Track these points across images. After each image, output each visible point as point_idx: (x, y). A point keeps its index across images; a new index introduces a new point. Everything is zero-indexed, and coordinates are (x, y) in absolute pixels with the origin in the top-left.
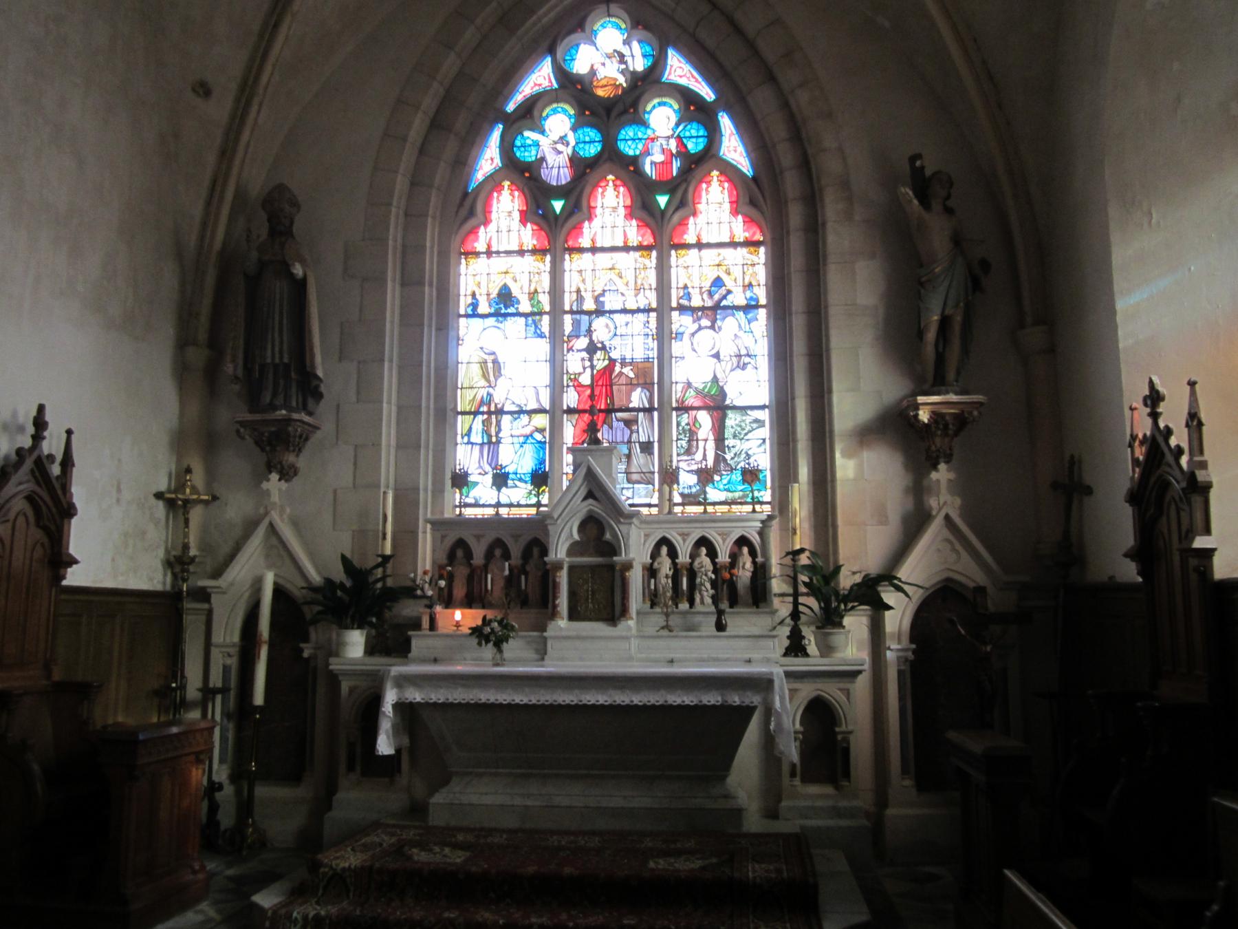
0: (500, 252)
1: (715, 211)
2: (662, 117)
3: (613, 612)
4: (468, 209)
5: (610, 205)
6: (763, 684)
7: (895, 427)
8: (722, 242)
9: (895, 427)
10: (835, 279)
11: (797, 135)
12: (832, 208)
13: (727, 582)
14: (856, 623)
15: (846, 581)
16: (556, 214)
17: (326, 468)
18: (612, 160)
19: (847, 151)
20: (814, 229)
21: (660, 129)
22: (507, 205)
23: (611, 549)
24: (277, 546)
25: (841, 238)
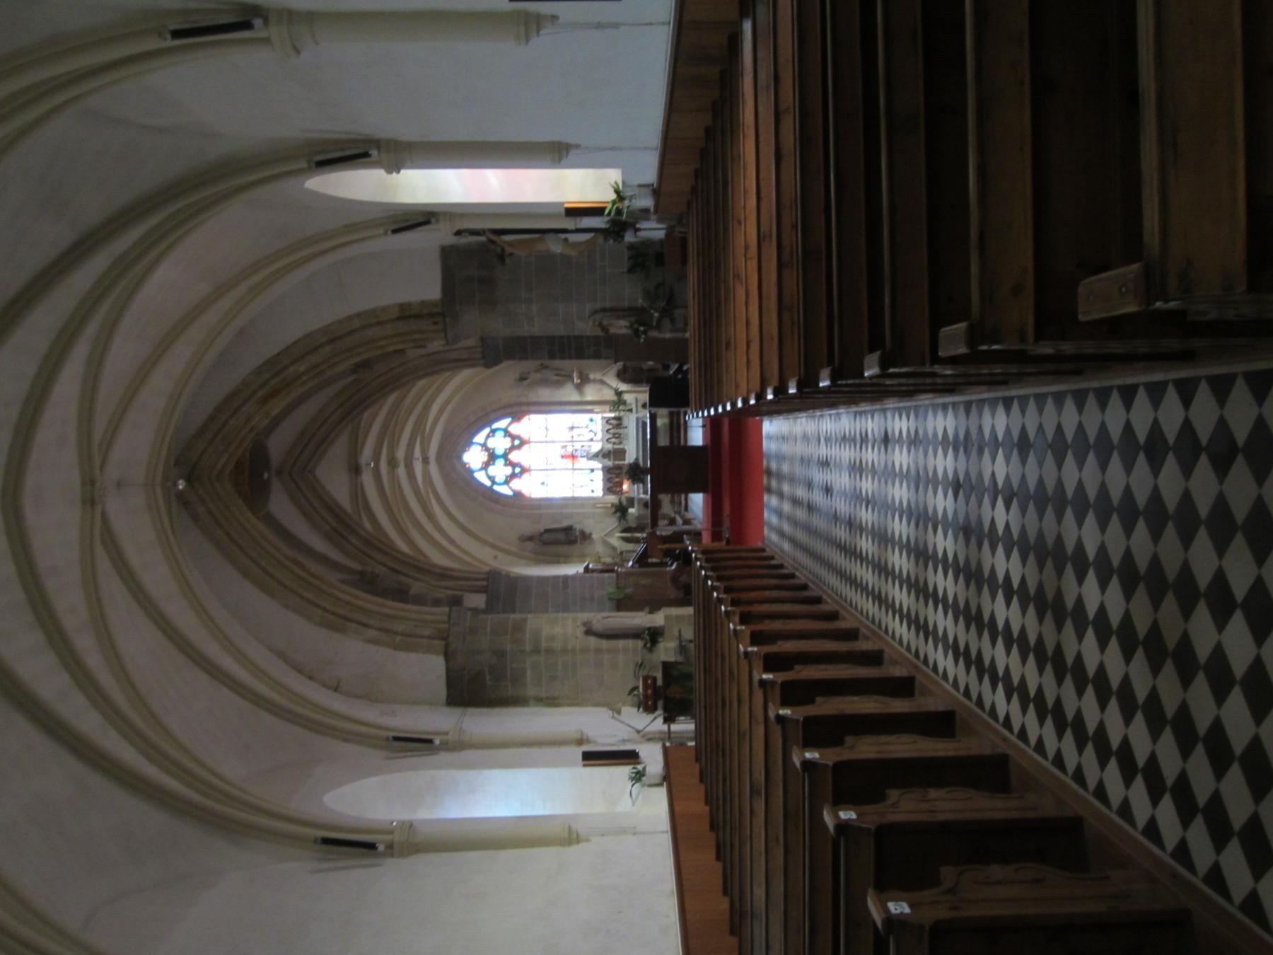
0: (531, 487)
1: (516, 429)
2: (491, 443)
3: (623, 452)
4: (518, 494)
5: (514, 457)
6: (638, 419)
7: (579, 387)
8: (530, 425)
9: (579, 387)
10: (543, 399)
11: (500, 409)
12: (524, 400)
13: (615, 426)
14: (626, 397)
15: (615, 398)
16: (519, 471)
17: (589, 525)
18: (505, 456)
19: (509, 395)
20: (529, 404)
21: (500, 444)
22: (517, 484)
23: (609, 452)
24: (610, 534)
25: (533, 398)
